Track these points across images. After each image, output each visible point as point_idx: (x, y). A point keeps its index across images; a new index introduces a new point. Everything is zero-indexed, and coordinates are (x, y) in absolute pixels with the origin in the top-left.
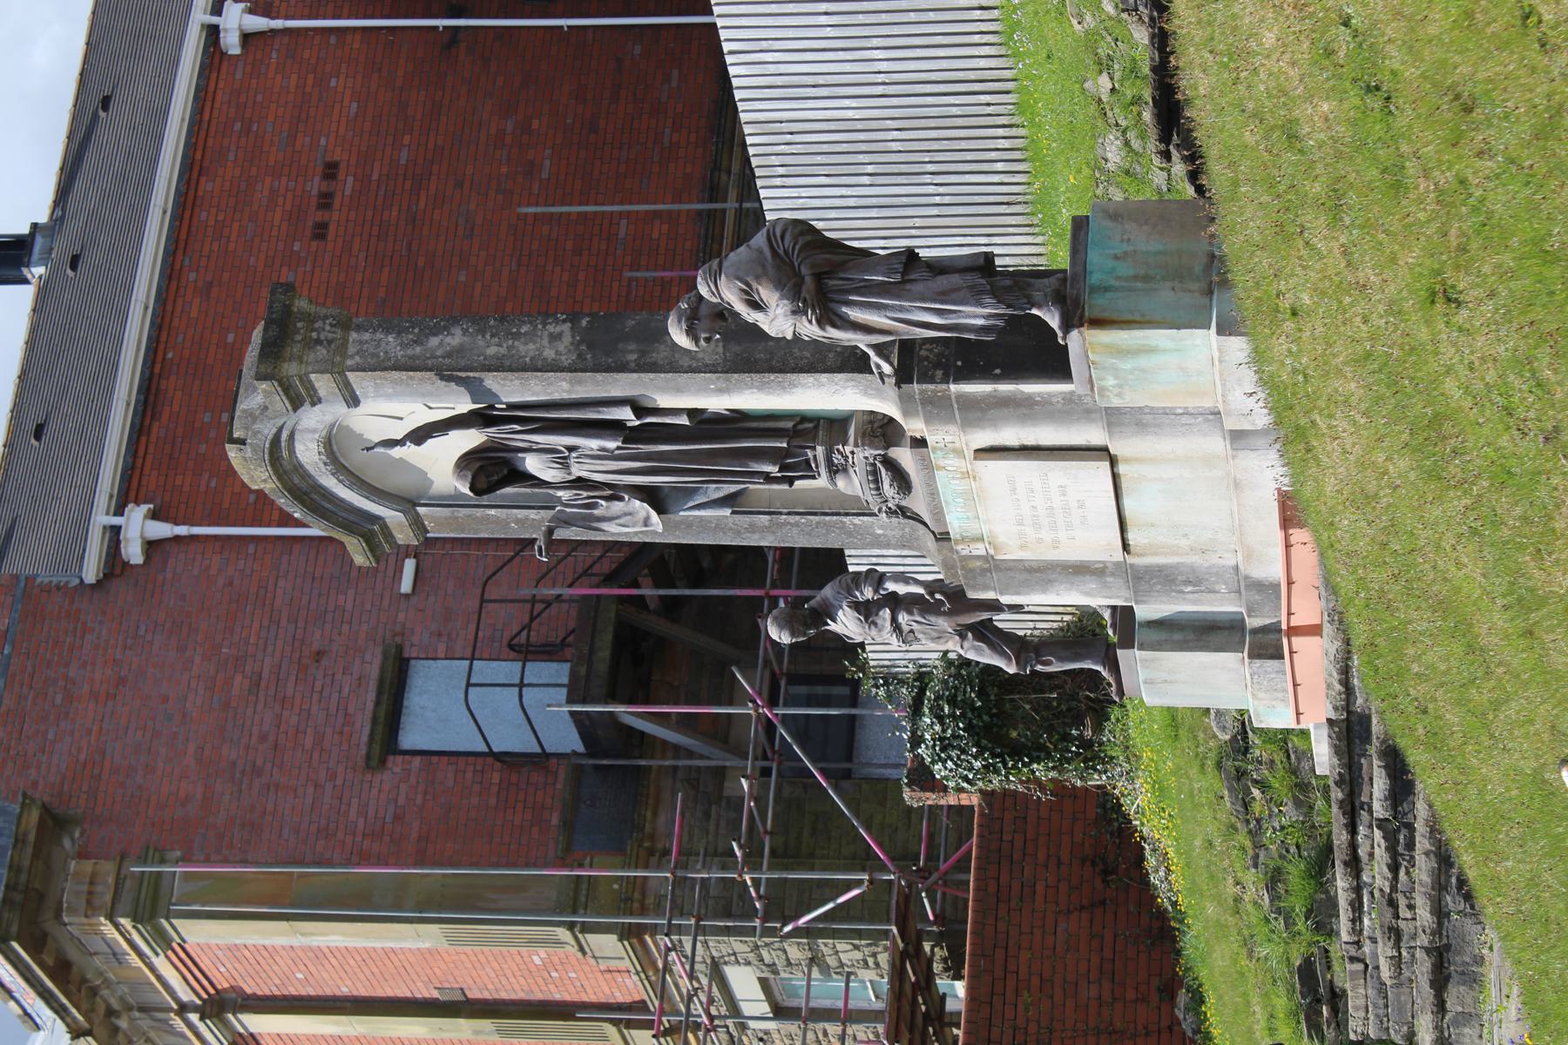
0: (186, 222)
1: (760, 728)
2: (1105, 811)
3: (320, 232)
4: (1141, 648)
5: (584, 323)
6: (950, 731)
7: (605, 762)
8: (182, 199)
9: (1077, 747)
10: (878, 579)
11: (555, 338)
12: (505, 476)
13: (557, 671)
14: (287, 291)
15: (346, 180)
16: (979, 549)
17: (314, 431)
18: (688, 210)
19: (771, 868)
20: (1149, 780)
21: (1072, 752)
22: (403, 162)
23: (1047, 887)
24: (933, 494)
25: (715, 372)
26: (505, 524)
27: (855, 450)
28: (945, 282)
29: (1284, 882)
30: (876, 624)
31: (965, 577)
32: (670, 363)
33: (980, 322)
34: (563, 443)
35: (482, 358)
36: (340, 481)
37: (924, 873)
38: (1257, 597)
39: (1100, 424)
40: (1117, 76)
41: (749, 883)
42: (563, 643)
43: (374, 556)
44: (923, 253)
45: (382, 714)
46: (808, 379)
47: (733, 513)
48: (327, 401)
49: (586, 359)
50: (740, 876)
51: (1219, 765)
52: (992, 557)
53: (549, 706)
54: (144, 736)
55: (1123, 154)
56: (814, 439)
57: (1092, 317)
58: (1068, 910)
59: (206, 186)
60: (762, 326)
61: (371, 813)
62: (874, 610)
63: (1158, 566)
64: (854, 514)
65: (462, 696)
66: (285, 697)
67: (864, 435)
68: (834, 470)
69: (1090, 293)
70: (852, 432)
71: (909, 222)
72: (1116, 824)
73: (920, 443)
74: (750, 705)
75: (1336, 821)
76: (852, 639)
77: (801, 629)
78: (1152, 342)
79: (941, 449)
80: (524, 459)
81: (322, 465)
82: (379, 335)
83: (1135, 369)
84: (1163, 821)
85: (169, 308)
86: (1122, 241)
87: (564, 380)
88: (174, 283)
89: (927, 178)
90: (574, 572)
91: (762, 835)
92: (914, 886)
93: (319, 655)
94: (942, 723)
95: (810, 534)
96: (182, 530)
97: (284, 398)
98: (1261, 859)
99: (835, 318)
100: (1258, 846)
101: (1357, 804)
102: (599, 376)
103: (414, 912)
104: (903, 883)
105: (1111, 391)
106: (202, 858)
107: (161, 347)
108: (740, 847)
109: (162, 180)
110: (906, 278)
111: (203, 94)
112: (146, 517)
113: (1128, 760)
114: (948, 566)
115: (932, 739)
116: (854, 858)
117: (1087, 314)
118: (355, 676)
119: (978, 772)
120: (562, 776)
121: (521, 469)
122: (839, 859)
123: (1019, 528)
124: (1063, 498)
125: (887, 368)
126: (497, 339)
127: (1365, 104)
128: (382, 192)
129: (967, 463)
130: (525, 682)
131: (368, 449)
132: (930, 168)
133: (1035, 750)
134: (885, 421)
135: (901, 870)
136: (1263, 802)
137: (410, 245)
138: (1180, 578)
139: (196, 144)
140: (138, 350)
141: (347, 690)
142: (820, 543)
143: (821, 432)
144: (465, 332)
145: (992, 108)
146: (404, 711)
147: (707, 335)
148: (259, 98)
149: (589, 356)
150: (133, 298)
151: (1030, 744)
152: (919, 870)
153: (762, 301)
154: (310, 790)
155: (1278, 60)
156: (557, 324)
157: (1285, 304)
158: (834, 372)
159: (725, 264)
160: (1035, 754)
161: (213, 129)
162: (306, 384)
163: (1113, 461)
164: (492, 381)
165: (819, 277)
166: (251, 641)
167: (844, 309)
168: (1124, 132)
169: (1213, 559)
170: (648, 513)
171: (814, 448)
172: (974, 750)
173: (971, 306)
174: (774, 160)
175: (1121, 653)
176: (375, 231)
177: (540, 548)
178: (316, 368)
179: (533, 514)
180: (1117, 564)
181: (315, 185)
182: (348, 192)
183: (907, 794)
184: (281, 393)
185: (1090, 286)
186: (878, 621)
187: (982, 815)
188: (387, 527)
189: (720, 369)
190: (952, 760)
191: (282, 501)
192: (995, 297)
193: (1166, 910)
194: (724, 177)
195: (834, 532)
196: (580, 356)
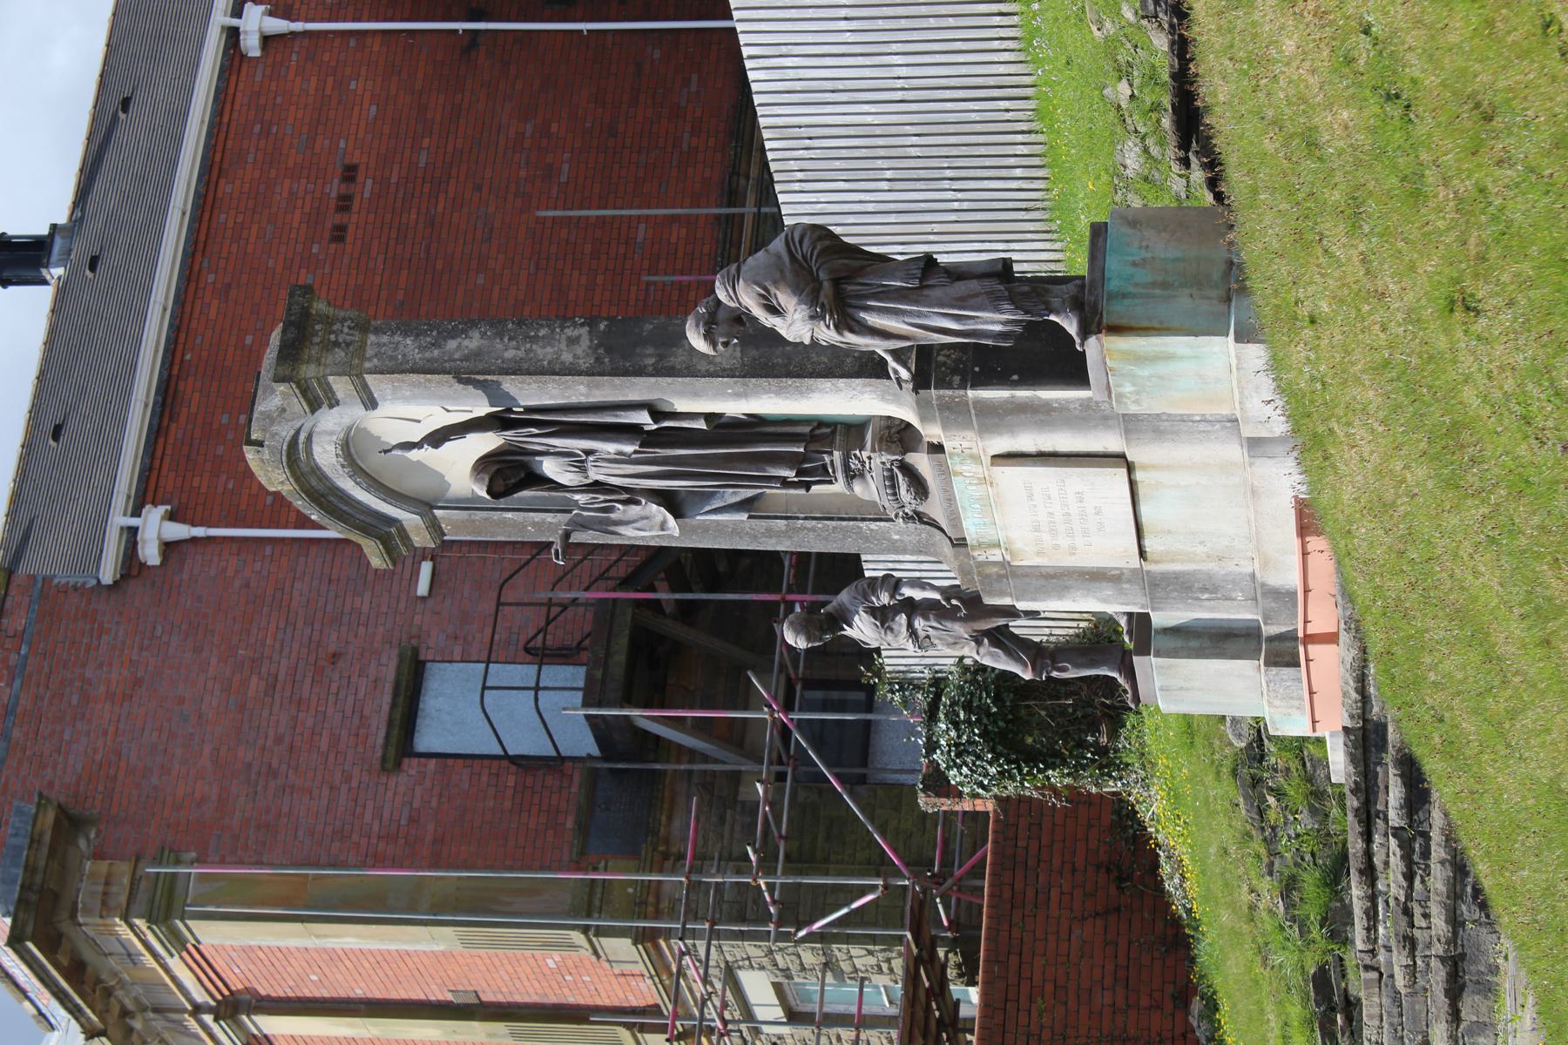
1: (775, 732)
3: (339, 234)
4: (1157, 655)
7: (620, 766)
8: (201, 201)
11: (573, 341)
14: (306, 293)
16: (996, 555)
17: (332, 433)
19: (785, 873)
21: (1087, 758)
22: (422, 165)
23: (1062, 893)
24: (950, 500)
25: (733, 377)
26: (522, 527)
28: (963, 288)
29: (1299, 890)
30: (892, 630)
31: (982, 583)
32: (688, 368)
33: (998, 328)
34: (580, 447)
35: (500, 361)
36: (357, 483)
37: (938, 879)
38: (1273, 605)
40: (1137, 82)
41: (764, 887)
43: (391, 559)
44: (941, 259)
45: (398, 716)
46: (826, 384)
47: (750, 517)
48: (345, 403)
49: (603, 363)
50: (755, 880)
53: (565, 709)
55: (1142, 160)
56: (831, 444)
59: (226, 188)
60: (780, 331)
61: (386, 815)
62: (891, 615)
63: (1175, 573)
64: (870, 520)
65: (478, 699)
67: (881, 440)
68: (851, 475)
69: (1107, 300)
72: (1131, 831)
73: (937, 448)
74: (766, 709)
76: (868, 644)
77: (817, 633)
78: (1171, 349)
79: (958, 455)
80: (542, 462)
82: (397, 338)
83: (1151, 376)
84: (1178, 828)
85: (188, 309)
86: (1140, 248)
87: (582, 383)
88: (193, 285)
89: (946, 184)
90: (591, 576)
91: (777, 840)
92: (929, 892)
93: (335, 657)
94: (957, 729)
95: (826, 539)
96: (199, 532)
97: (302, 400)
98: (1277, 867)
100: (1273, 854)
101: (1373, 812)
102: (617, 380)
105: (1129, 398)
106: (217, 859)
107: (180, 347)
108: (755, 852)
110: (924, 284)
112: (264, 14)
114: (964, 572)
116: (869, 864)
117: (1105, 320)
119: (993, 778)
120: (577, 779)
122: (853, 864)
124: (1079, 504)
125: (904, 374)
126: (514, 343)
128: (400, 195)
129: (985, 469)
131: (386, 452)
132: (949, 174)
134: (903, 426)
136: (1279, 810)
138: (1196, 585)
140: (156, 351)
143: (838, 437)
144: (483, 335)
145: (1011, 114)
146: (420, 713)
147: (725, 340)
148: (279, 100)
149: (607, 360)
151: (1045, 750)
152: (934, 875)
154: (326, 792)
155: (1298, 68)
156: (575, 328)
157: (1304, 312)
159: (744, 268)
163: (1130, 468)
164: (510, 385)
165: (837, 282)
166: (268, 642)
167: (862, 315)
168: (1143, 139)
171: (831, 453)
172: (990, 756)
173: (989, 311)
174: (793, 165)
176: (394, 235)
179: (549, 517)
180: (1134, 571)
181: (334, 188)
183: (922, 800)
184: (299, 395)
186: (894, 627)
187: (997, 821)
189: (737, 374)
190: (967, 766)
191: (300, 503)
194: (742, 181)
196: (597, 359)
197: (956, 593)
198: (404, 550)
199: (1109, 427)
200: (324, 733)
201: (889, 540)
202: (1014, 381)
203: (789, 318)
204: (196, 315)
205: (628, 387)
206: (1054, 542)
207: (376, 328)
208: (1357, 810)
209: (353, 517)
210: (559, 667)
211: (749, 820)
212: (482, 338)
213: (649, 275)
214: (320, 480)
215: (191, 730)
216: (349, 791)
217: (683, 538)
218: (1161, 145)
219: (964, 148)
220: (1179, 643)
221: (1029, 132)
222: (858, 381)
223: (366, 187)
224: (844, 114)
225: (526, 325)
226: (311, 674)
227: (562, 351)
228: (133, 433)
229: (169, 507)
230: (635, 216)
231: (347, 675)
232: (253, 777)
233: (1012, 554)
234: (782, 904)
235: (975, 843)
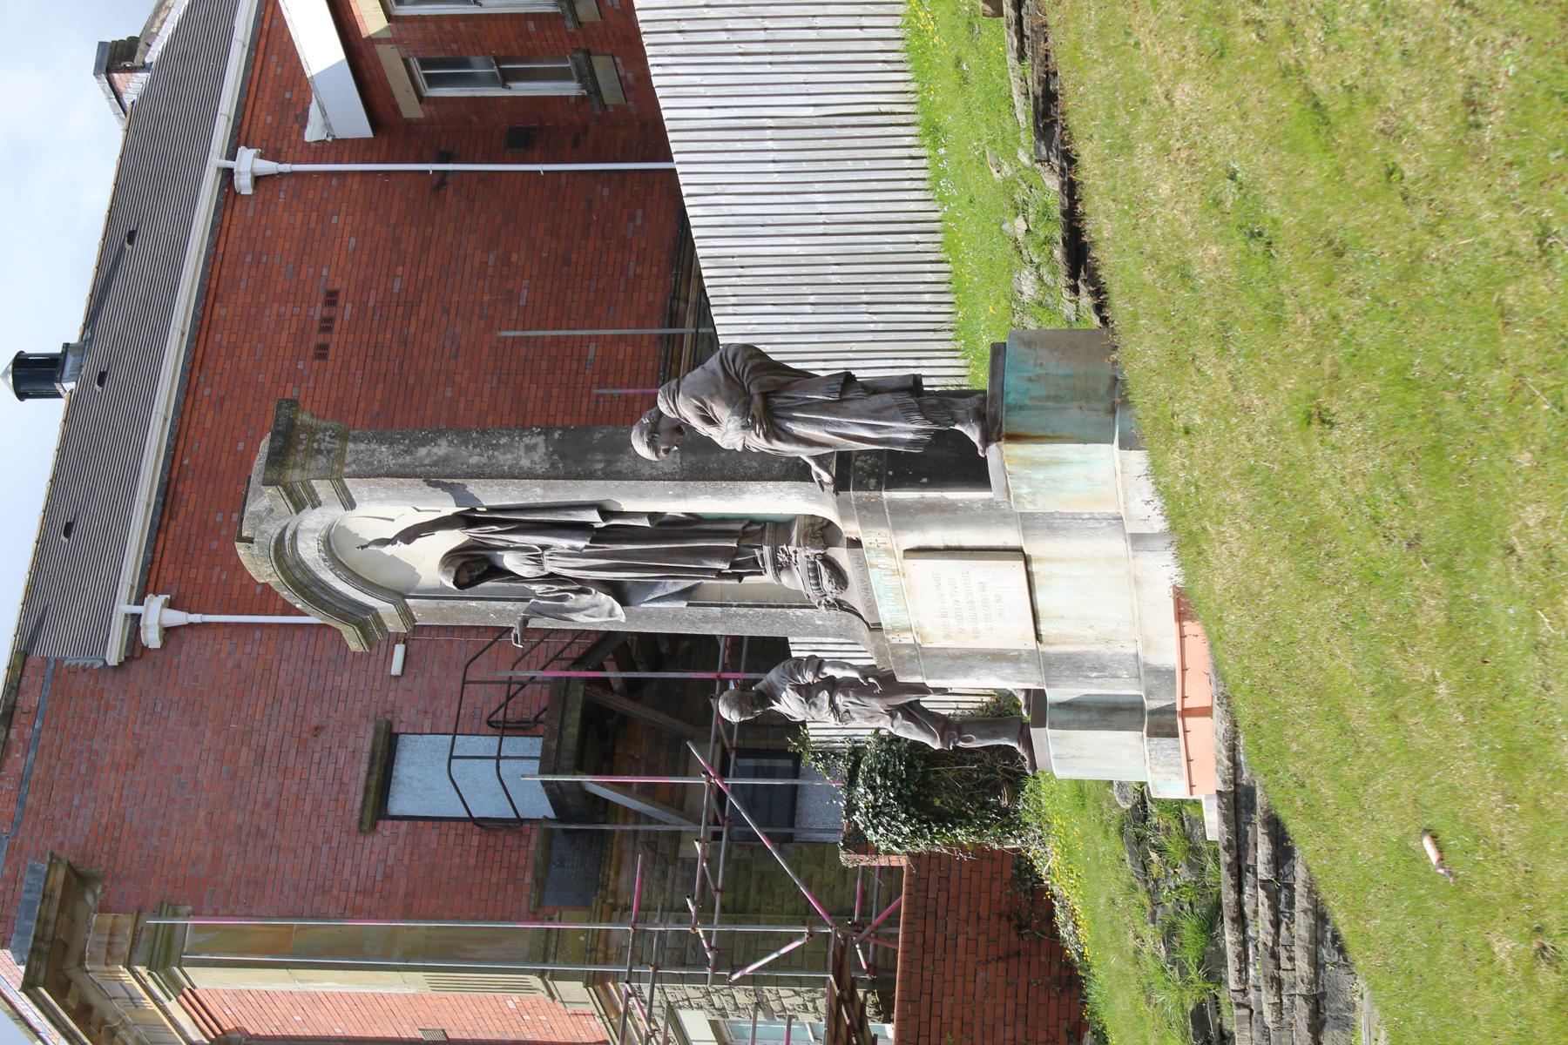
0: (202, 344)
1: (712, 797)
2: (1020, 872)
3: (322, 352)
4: (1052, 727)
7: (573, 827)
8: (199, 323)
10: (818, 665)
11: (530, 449)
14: (292, 406)
16: (908, 639)
17: (315, 531)
22: (396, 290)
24: (867, 589)
29: (1179, 936)
30: (815, 705)
31: (895, 662)
32: (632, 472)
33: (909, 436)
36: (337, 576)
37: (858, 927)
38: (1154, 682)
40: (1031, 218)
41: (702, 935)
42: (536, 721)
43: (367, 643)
45: (373, 783)
47: (689, 605)
50: (694, 929)
51: (1121, 832)
53: (523, 776)
55: (1037, 287)
56: (761, 540)
59: (221, 311)
61: (363, 872)
62: (814, 692)
63: (1066, 654)
64: (796, 607)
65: (446, 767)
67: (805, 536)
68: (779, 568)
69: (1007, 411)
71: (847, 347)
73: (855, 544)
74: (704, 776)
79: (874, 549)
80: (502, 556)
82: (373, 446)
83: (1046, 479)
85: (186, 420)
86: (1035, 365)
87: (539, 486)
88: (191, 397)
89: (863, 308)
92: (849, 938)
93: (318, 730)
95: (757, 624)
96: (196, 618)
97: (288, 501)
98: (1159, 915)
100: (1156, 903)
102: (569, 483)
106: (211, 912)
107: (179, 454)
112: (163, 606)
114: (880, 653)
117: (1004, 430)
118: (350, 749)
120: (534, 839)
121: (499, 565)
125: (826, 478)
127: (1249, 248)
128: (377, 317)
129: (898, 562)
131: (363, 547)
132: (865, 298)
133: (958, 818)
137: (401, 367)
140: (158, 456)
141: (342, 763)
144: (450, 443)
145: (921, 245)
148: (268, 233)
149: (560, 465)
153: (715, 416)
154: (309, 851)
156: (532, 436)
157: (1179, 423)
159: (683, 384)
160: (957, 821)
163: (1027, 561)
164: (474, 487)
165: (766, 396)
167: (789, 425)
168: (1037, 268)
170: (612, 605)
171: (761, 548)
173: (901, 422)
174: (727, 291)
176: (371, 351)
178: (317, 475)
179: (509, 606)
180: (1031, 652)
181: (318, 311)
182: (347, 317)
184: (285, 497)
187: (910, 875)
188: (379, 617)
190: (883, 826)
194: (682, 305)
196: (553, 465)
199: (1009, 524)
201: (814, 625)
204: (193, 424)
208: (1230, 865)
210: (518, 738)
211: (688, 875)
212: (449, 446)
213: (598, 388)
215: (187, 796)
218: (1054, 274)
223: (347, 310)
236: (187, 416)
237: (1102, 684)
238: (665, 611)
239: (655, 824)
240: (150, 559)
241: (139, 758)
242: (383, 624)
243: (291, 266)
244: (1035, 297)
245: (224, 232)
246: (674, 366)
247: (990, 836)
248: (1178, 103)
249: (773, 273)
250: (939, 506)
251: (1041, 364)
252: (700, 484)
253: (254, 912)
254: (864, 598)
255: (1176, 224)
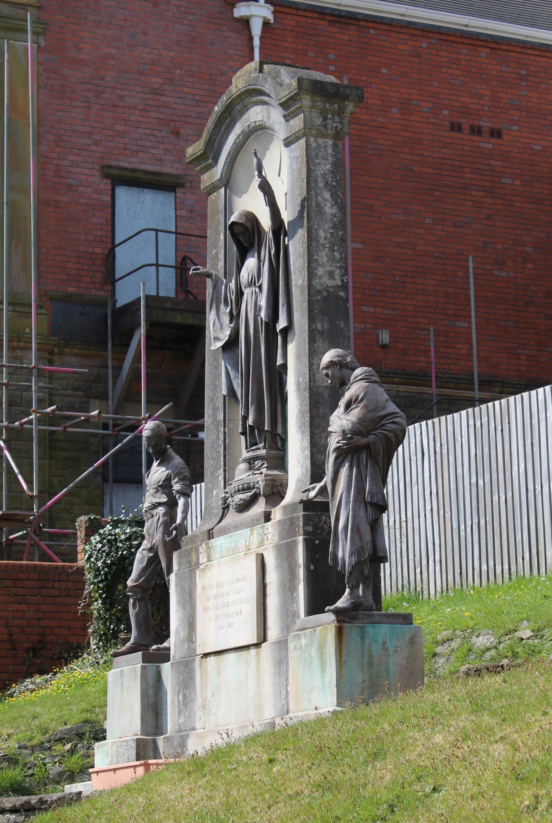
0: (459, 40)
1: (133, 422)
2: (75, 649)
3: (456, 128)
4: (143, 668)
5: (342, 294)
6: (121, 545)
7: (109, 321)
8: (474, 37)
9: (113, 629)
10: (186, 494)
11: (331, 275)
12: (242, 245)
13: (170, 289)
14: (359, 97)
15: (490, 143)
16: (203, 559)
17: (269, 118)
18: (473, 366)
19: (39, 431)
20: (90, 676)
21: (110, 625)
22: (503, 180)
23: (24, 612)
24: (237, 527)
25: (310, 381)
26: (215, 246)
27: (263, 475)
28: (366, 531)
29: (9, 767)
31: (186, 550)
32: (315, 351)
33: (340, 555)
34: (264, 282)
35: (317, 227)
36: (238, 136)
37: (38, 531)
38: (176, 743)
39: (280, 636)
40: (530, 642)
41: (31, 417)
42: (188, 292)
43: (192, 160)
44: (385, 515)
45: (138, 175)
46: (307, 443)
47: (225, 396)
48: (287, 126)
49: (317, 295)
50: (34, 411)
51: (86, 722)
52: (198, 567)
53: (144, 283)
54: (120, 20)
55: (482, 647)
56: (271, 448)
57: (344, 628)
58: (8, 626)
59: (484, 53)
60: (336, 411)
61: (73, 169)
62: (166, 491)
63: (194, 677)
64: (225, 476)
65: (152, 227)
66: (148, 111)
67: (273, 480)
68: (250, 461)
69: (360, 626)
70: (275, 472)
71: (447, 509)
72: (66, 656)
73: (267, 517)
74: (147, 415)
75: (18, 800)
76: (148, 477)
77: (152, 443)
78: (328, 669)
79: (263, 532)
80: (254, 257)
81: (248, 124)
82: (330, 159)
83: (311, 657)
84: (63, 686)
85: (403, 30)
86: (395, 647)
87: (303, 282)
88: (419, 33)
89: (475, 520)
90: (197, 294)
91: (63, 425)
92: (29, 525)
93: (177, 133)
94: (126, 540)
95: (212, 447)
96: (257, 42)
97: (287, 97)
98: (24, 751)
99: (341, 459)
100: (33, 749)
101: (29, 813)
102: (306, 304)
103: (7, 199)
104: (31, 518)
105: (298, 643)
106: (40, 60)
107: (378, 26)
108: (53, 411)
109: (487, 24)
110: (368, 505)
111: (544, 49)
112: (264, 18)
113: (105, 662)
114: (194, 537)
115: (116, 533)
116: (50, 486)
117: (346, 625)
118: (163, 157)
119: (95, 564)
120: (100, 293)
121: (248, 255)
122: (49, 476)
123: (216, 585)
124: (234, 613)
125: (312, 494)
126: (329, 236)
127: (383, 804)
128: (482, 167)
129: (255, 549)
130: (160, 268)
131: (255, 153)
132: (482, 522)
133: (110, 602)
134: (283, 495)
135: (40, 516)
136: (62, 751)
137: (446, 186)
138: (187, 692)
139: (512, 45)
140: (375, 11)
141: (153, 152)
142: (207, 454)
143: (275, 452)
144: (334, 215)
145: (521, 561)
146: (141, 189)
147: (330, 375)
148: (543, 86)
149: (319, 297)
150: (408, 7)
151: (114, 598)
152: (40, 528)
153: (351, 410)
154: (87, 129)
155: (423, 745)
156: (340, 276)
157: (279, 756)
158: (311, 460)
159: (375, 386)
160: (108, 601)
161: (521, 56)
162: (297, 112)
163: (257, 645)
164: (301, 234)
165: (367, 447)
166: (185, 89)
167: (347, 464)
168: (496, 648)
169: (199, 714)
170: (222, 340)
171: (264, 448)
172: (109, 562)
173: (350, 548)
174: (485, 419)
175: (139, 655)
176: (456, 163)
177: (198, 269)
178: (307, 118)
179: (221, 264)
180: (195, 650)
181: (486, 124)
182: (482, 145)
183: (83, 518)
184: (290, 95)
185: (365, 626)
187: (71, 567)
188: (211, 168)
189: (312, 384)
190: (102, 547)
191: (225, 99)
192: (357, 564)
193: (9, 690)
194: (498, 389)
195: (214, 463)
196: (319, 291)
197: (181, 532)
198: (199, 168)
199: (282, 631)
200: (125, 127)
201: (213, 488)
202: (310, 566)
203: (343, 416)
204: (400, 36)
205: (302, 312)
206: (211, 597)
207: (337, 145)
208: (29, 803)
209: (218, 134)
210: (174, 279)
211: (76, 407)
212: (332, 215)
213: (434, 330)
214: (240, 111)
215: (125, 40)
216: (88, 145)
217: (211, 352)
218: (491, 659)
219: (499, 531)
220: (151, 681)
221: (510, 574)
222: (309, 464)
223: (487, 145)
224: (518, 452)
225: (341, 244)
226: (164, 118)
227: (325, 268)
228: (423, 13)
229: (272, 22)
230: (471, 320)
231: (165, 141)
232: (95, 82)
233: (203, 569)
234: (21, 430)
235: (65, 554)
236: (406, 31)
237: (174, 704)
238: (219, 380)
239: (113, 381)
240: (299, 7)
241: (152, 4)
242: (206, 171)
243: (519, 103)
244: (475, 647)
245: (543, 54)
246: (452, 385)
247: (98, 626)
248: (495, 746)
249: (499, 453)
250: (294, 579)
251: (396, 652)
252: (307, 401)
253: (41, 91)
254: (230, 525)
255: (412, 748)
